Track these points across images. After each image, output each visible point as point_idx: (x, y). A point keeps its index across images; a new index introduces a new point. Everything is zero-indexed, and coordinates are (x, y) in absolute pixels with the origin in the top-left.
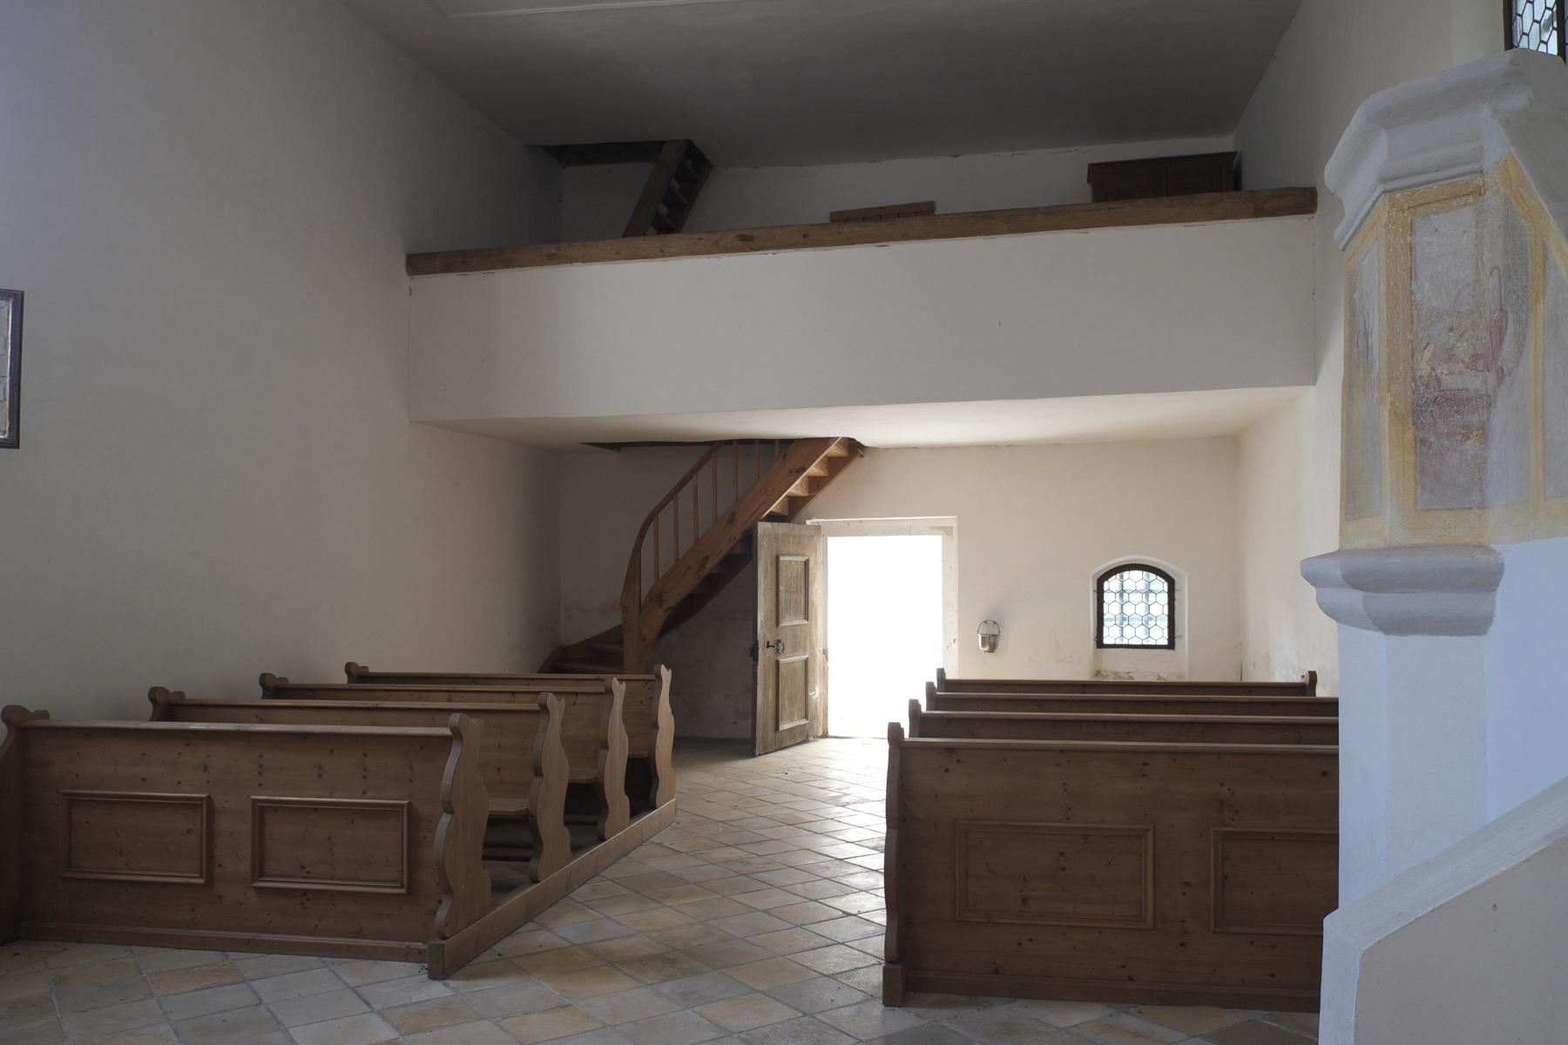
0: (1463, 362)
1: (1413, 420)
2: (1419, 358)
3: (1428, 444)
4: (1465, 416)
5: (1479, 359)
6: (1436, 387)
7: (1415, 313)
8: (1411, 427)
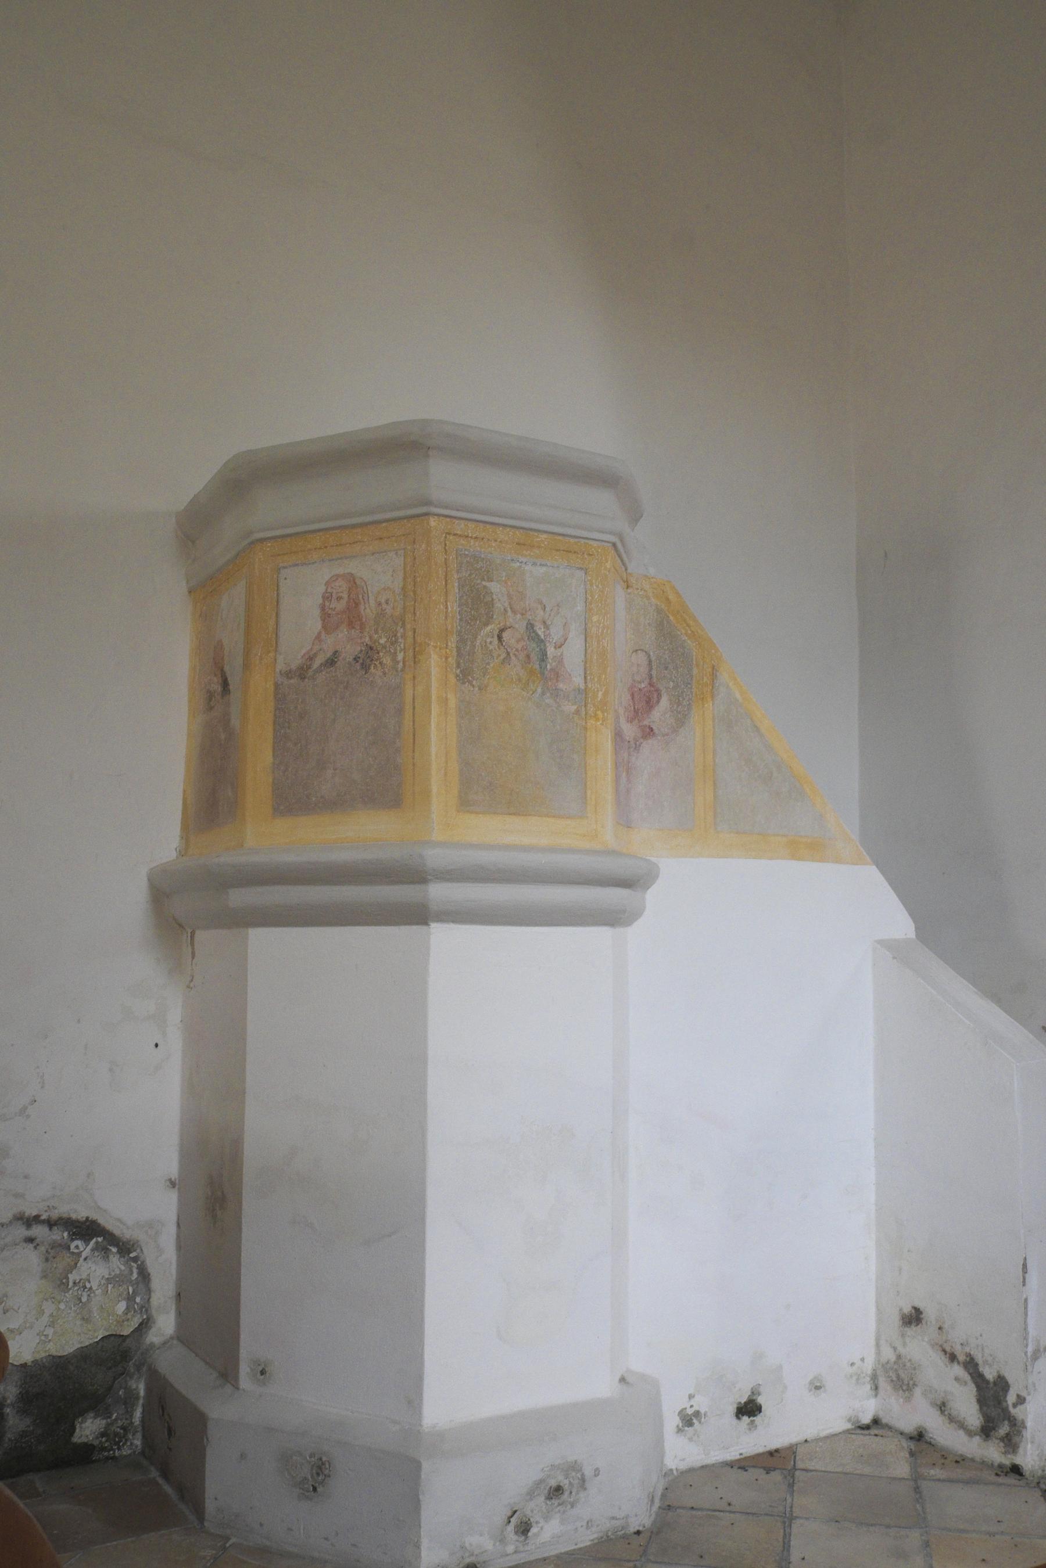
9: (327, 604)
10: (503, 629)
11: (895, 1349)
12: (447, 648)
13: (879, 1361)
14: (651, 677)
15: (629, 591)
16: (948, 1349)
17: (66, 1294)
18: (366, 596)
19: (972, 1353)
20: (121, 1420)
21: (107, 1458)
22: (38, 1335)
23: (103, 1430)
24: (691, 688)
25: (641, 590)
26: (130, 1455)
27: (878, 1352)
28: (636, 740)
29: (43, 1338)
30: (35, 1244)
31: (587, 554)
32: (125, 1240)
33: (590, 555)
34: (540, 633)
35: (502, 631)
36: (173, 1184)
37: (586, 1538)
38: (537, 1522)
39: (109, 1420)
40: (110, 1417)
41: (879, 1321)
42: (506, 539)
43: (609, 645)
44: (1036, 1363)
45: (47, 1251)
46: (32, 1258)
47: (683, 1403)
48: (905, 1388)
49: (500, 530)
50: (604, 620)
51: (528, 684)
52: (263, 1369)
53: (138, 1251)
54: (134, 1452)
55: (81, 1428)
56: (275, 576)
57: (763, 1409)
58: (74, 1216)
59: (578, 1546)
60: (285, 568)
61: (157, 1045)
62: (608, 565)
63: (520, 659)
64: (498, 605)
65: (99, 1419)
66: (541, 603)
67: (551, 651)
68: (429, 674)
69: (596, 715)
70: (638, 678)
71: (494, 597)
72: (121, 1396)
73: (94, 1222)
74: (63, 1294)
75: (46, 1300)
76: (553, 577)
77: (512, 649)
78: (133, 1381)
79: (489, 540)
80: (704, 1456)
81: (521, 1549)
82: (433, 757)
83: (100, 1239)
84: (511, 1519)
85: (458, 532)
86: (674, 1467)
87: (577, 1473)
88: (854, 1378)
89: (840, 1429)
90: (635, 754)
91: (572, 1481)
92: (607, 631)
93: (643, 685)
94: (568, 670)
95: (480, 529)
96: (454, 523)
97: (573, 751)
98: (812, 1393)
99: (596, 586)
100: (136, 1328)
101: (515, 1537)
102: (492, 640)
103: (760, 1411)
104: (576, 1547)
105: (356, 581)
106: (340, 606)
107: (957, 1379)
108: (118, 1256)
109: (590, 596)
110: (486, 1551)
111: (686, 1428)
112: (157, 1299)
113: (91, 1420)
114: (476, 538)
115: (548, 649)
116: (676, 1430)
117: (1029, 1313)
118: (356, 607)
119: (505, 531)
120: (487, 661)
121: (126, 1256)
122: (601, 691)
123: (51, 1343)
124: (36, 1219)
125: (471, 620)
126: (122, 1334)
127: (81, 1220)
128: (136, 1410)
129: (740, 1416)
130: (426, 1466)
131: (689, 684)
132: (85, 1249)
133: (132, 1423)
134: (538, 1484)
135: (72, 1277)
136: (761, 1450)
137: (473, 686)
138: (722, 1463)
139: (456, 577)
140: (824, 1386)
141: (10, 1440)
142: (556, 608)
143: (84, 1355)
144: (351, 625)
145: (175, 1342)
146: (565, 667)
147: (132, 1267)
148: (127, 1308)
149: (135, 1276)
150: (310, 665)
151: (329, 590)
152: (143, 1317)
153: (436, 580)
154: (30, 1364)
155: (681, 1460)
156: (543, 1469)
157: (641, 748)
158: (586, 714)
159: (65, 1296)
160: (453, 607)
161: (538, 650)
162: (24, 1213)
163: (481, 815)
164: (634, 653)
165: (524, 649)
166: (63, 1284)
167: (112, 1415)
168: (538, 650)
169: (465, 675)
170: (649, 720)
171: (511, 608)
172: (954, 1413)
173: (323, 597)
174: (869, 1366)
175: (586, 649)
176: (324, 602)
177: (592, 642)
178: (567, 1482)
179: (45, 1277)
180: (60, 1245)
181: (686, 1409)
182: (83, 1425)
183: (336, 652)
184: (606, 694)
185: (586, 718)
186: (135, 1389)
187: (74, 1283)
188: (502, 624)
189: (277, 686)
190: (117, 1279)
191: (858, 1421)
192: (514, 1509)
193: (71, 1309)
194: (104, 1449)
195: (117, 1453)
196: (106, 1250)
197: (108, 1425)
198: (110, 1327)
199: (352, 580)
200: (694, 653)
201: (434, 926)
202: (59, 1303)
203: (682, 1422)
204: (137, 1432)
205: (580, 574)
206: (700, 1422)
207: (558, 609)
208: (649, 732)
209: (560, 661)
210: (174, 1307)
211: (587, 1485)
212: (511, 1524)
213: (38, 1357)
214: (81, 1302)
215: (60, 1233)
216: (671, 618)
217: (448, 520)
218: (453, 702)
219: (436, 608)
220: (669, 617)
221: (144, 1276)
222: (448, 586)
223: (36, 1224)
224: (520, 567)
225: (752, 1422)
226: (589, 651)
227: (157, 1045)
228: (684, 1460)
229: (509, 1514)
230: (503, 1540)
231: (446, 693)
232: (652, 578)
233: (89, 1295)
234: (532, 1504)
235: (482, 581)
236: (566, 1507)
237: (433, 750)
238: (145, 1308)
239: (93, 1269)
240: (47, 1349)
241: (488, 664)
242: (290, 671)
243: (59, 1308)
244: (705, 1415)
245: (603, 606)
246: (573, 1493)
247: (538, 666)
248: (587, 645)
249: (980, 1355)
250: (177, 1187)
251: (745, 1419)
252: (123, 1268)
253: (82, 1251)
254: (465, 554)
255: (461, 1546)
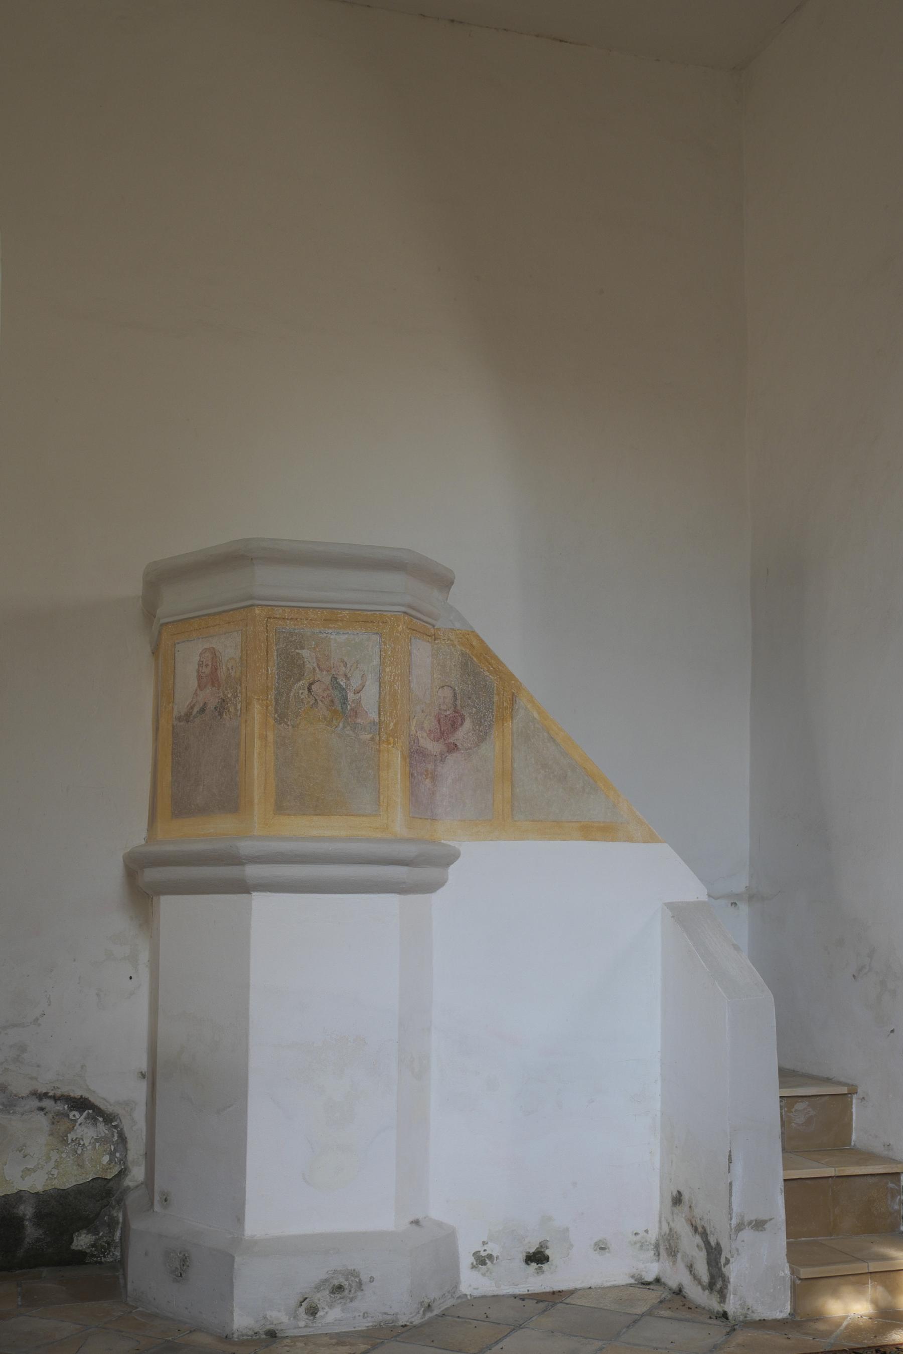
9: (201, 669)
10: (312, 683)
11: (669, 1223)
12: (267, 700)
13: (661, 1233)
14: (455, 706)
15: (436, 642)
16: (694, 1223)
17: (67, 1148)
18: (221, 664)
19: (705, 1225)
20: (106, 1237)
21: (96, 1262)
22: (47, 1173)
23: (93, 1242)
24: (492, 712)
25: (448, 640)
26: (112, 1262)
27: (660, 1228)
28: (441, 754)
29: (50, 1176)
30: (45, 1112)
31: (382, 623)
32: (108, 1113)
33: (383, 622)
34: (342, 683)
35: (311, 684)
36: (143, 1076)
37: (363, 1325)
38: (323, 1308)
39: (97, 1236)
40: (98, 1235)
41: (662, 1202)
42: (316, 617)
43: (400, 688)
44: (739, 1234)
45: (53, 1117)
46: (43, 1121)
47: (478, 1247)
48: (673, 1254)
49: (310, 612)
50: (396, 669)
51: (332, 721)
52: (166, 1198)
53: (118, 1121)
54: (115, 1260)
55: (77, 1239)
56: (173, 649)
57: (550, 1260)
58: (72, 1095)
59: (356, 1329)
60: (178, 643)
61: (131, 978)
62: (400, 628)
63: (326, 703)
64: (308, 666)
65: (90, 1235)
66: (343, 661)
67: (351, 696)
68: (254, 718)
69: (388, 740)
70: (444, 707)
71: (305, 660)
72: (106, 1220)
73: (86, 1099)
74: (64, 1147)
75: (53, 1150)
76: (353, 642)
77: (319, 697)
78: (114, 1211)
79: (301, 619)
80: (495, 1289)
81: (311, 1325)
82: (255, 777)
83: (91, 1111)
84: (303, 1304)
85: (277, 616)
86: (468, 1293)
87: (355, 1278)
88: (638, 1245)
89: (624, 1283)
90: (441, 765)
91: (351, 1283)
92: (398, 678)
94: (365, 709)
95: (294, 612)
96: (274, 610)
98: (597, 1252)
99: (389, 645)
100: (116, 1175)
101: (306, 1317)
102: (303, 691)
103: (548, 1261)
104: (354, 1329)
105: (216, 653)
106: (207, 671)
107: (698, 1246)
108: (104, 1124)
109: (384, 653)
110: (282, 1323)
111: (480, 1266)
112: (131, 1156)
113: (84, 1235)
114: (291, 619)
115: (348, 695)
116: (470, 1266)
117: (734, 1194)
118: (215, 671)
119: (314, 612)
120: (299, 707)
121: (109, 1124)
122: (392, 722)
123: (56, 1180)
124: (46, 1095)
125: (287, 678)
126: (106, 1178)
127: (77, 1097)
128: (117, 1231)
129: (529, 1262)
130: (237, 1259)
131: (491, 709)
132: (80, 1118)
133: (113, 1240)
134: (323, 1282)
135: (70, 1136)
136: (548, 1290)
137: (288, 725)
138: (511, 1295)
139: (275, 648)
140: (608, 1248)
141: (28, 1243)
142: (355, 664)
143: (80, 1191)
144: (213, 684)
145: (143, 1186)
146: (362, 707)
147: (114, 1132)
148: (110, 1160)
149: (116, 1138)
150: (192, 712)
151: (202, 660)
152: (121, 1167)
153: (259, 652)
154: (41, 1193)
155: (474, 1289)
156: (328, 1272)
158: (380, 740)
159: (65, 1148)
160: (273, 670)
161: (340, 696)
162: (37, 1090)
163: (293, 816)
165: (328, 696)
166: (64, 1141)
167: (99, 1233)
168: (340, 696)
169: (281, 718)
171: (319, 667)
172: (696, 1273)
173: (198, 664)
174: (653, 1236)
175: (380, 692)
176: (199, 667)
177: (385, 687)
178: (347, 1283)
179: (52, 1134)
180: (62, 1114)
181: (480, 1251)
182: (79, 1238)
183: (205, 703)
184: (395, 725)
185: (379, 743)
186: (116, 1217)
187: (72, 1140)
188: (311, 679)
189: (173, 726)
190: (103, 1140)
191: (641, 1278)
192: (306, 1297)
193: (70, 1157)
194: (94, 1256)
195: (103, 1259)
196: (95, 1119)
197: (97, 1240)
198: (98, 1172)
199: (213, 652)
201: (255, 894)
202: (62, 1153)
203: (476, 1261)
204: (117, 1246)
205: (376, 638)
206: (492, 1263)
207: (357, 665)
208: (453, 748)
209: (359, 703)
210: (144, 1162)
211: (363, 1287)
212: (302, 1307)
213: (47, 1188)
214: (77, 1153)
215: (62, 1105)
217: (269, 608)
218: (271, 737)
219: (260, 672)
220: (472, 658)
221: (123, 1139)
222: (268, 655)
223: (46, 1098)
224: (327, 637)
225: (540, 1268)
226: (383, 694)
227: (131, 978)
228: (477, 1289)
229: (301, 1299)
230: (296, 1317)
231: (266, 732)
232: (458, 630)
233: (82, 1150)
234: (319, 1295)
235: (295, 649)
236: (346, 1301)
237: (256, 772)
238: (123, 1160)
239: (85, 1131)
240: (53, 1184)
241: (300, 708)
242: (181, 716)
243: (62, 1157)
244: (497, 1258)
245: (395, 660)
246: (352, 1292)
247: (341, 708)
248: (381, 689)
249: (708, 1227)
250: (146, 1078)
251: (534, 1265)
252: (107, 1132)
253: (78, 1119)
254: (282, 632)
255: (263, 1316)
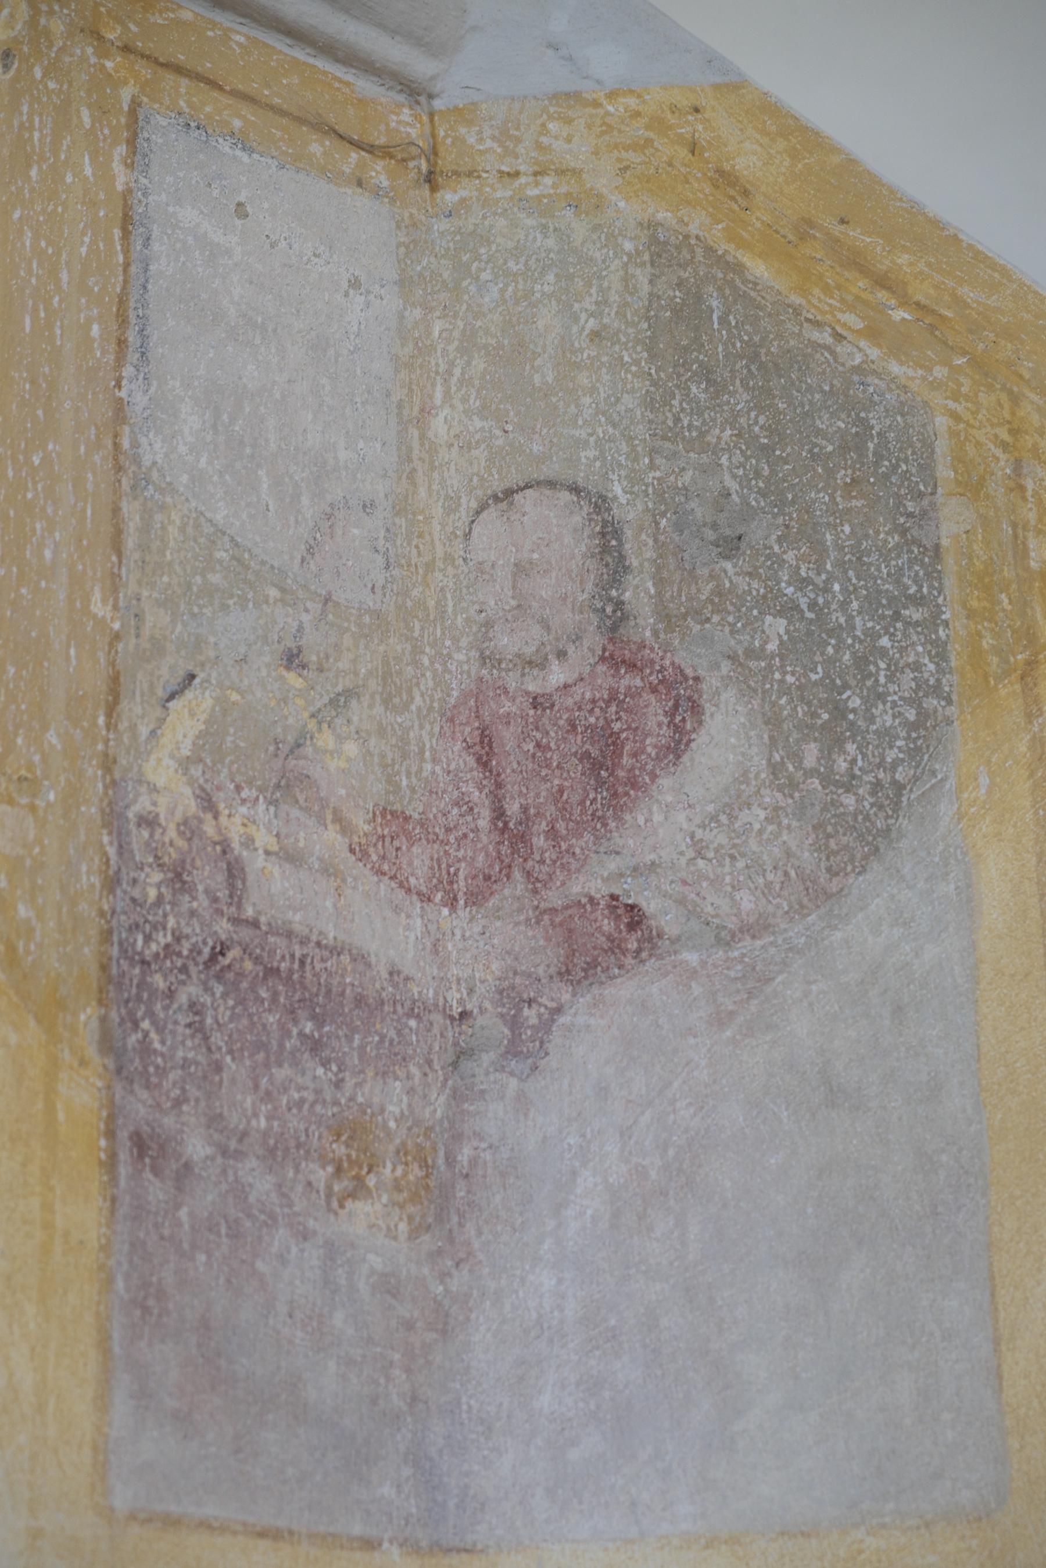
0: (345, 828)
1: (103, 1020)
2: (144, 731)
3: (173, 1166)
4: (350, 1083)
5: (412, 841)
6: (222, 894)
7: (130, 509)
8: (92, 1052)
24: (935, 620)
93: (557, 675)
97: (359, 609)
131: (918, 601)
157: (556, 1038)
164: (491, 514)
170: (613, 865)
200: (942, 422)
216: (758, 269)
220: (739, 268)
232: (612, 95)
